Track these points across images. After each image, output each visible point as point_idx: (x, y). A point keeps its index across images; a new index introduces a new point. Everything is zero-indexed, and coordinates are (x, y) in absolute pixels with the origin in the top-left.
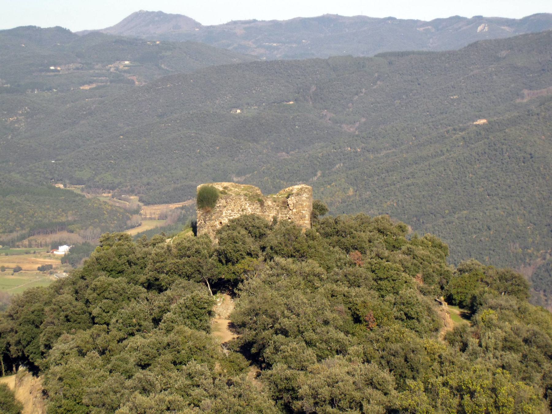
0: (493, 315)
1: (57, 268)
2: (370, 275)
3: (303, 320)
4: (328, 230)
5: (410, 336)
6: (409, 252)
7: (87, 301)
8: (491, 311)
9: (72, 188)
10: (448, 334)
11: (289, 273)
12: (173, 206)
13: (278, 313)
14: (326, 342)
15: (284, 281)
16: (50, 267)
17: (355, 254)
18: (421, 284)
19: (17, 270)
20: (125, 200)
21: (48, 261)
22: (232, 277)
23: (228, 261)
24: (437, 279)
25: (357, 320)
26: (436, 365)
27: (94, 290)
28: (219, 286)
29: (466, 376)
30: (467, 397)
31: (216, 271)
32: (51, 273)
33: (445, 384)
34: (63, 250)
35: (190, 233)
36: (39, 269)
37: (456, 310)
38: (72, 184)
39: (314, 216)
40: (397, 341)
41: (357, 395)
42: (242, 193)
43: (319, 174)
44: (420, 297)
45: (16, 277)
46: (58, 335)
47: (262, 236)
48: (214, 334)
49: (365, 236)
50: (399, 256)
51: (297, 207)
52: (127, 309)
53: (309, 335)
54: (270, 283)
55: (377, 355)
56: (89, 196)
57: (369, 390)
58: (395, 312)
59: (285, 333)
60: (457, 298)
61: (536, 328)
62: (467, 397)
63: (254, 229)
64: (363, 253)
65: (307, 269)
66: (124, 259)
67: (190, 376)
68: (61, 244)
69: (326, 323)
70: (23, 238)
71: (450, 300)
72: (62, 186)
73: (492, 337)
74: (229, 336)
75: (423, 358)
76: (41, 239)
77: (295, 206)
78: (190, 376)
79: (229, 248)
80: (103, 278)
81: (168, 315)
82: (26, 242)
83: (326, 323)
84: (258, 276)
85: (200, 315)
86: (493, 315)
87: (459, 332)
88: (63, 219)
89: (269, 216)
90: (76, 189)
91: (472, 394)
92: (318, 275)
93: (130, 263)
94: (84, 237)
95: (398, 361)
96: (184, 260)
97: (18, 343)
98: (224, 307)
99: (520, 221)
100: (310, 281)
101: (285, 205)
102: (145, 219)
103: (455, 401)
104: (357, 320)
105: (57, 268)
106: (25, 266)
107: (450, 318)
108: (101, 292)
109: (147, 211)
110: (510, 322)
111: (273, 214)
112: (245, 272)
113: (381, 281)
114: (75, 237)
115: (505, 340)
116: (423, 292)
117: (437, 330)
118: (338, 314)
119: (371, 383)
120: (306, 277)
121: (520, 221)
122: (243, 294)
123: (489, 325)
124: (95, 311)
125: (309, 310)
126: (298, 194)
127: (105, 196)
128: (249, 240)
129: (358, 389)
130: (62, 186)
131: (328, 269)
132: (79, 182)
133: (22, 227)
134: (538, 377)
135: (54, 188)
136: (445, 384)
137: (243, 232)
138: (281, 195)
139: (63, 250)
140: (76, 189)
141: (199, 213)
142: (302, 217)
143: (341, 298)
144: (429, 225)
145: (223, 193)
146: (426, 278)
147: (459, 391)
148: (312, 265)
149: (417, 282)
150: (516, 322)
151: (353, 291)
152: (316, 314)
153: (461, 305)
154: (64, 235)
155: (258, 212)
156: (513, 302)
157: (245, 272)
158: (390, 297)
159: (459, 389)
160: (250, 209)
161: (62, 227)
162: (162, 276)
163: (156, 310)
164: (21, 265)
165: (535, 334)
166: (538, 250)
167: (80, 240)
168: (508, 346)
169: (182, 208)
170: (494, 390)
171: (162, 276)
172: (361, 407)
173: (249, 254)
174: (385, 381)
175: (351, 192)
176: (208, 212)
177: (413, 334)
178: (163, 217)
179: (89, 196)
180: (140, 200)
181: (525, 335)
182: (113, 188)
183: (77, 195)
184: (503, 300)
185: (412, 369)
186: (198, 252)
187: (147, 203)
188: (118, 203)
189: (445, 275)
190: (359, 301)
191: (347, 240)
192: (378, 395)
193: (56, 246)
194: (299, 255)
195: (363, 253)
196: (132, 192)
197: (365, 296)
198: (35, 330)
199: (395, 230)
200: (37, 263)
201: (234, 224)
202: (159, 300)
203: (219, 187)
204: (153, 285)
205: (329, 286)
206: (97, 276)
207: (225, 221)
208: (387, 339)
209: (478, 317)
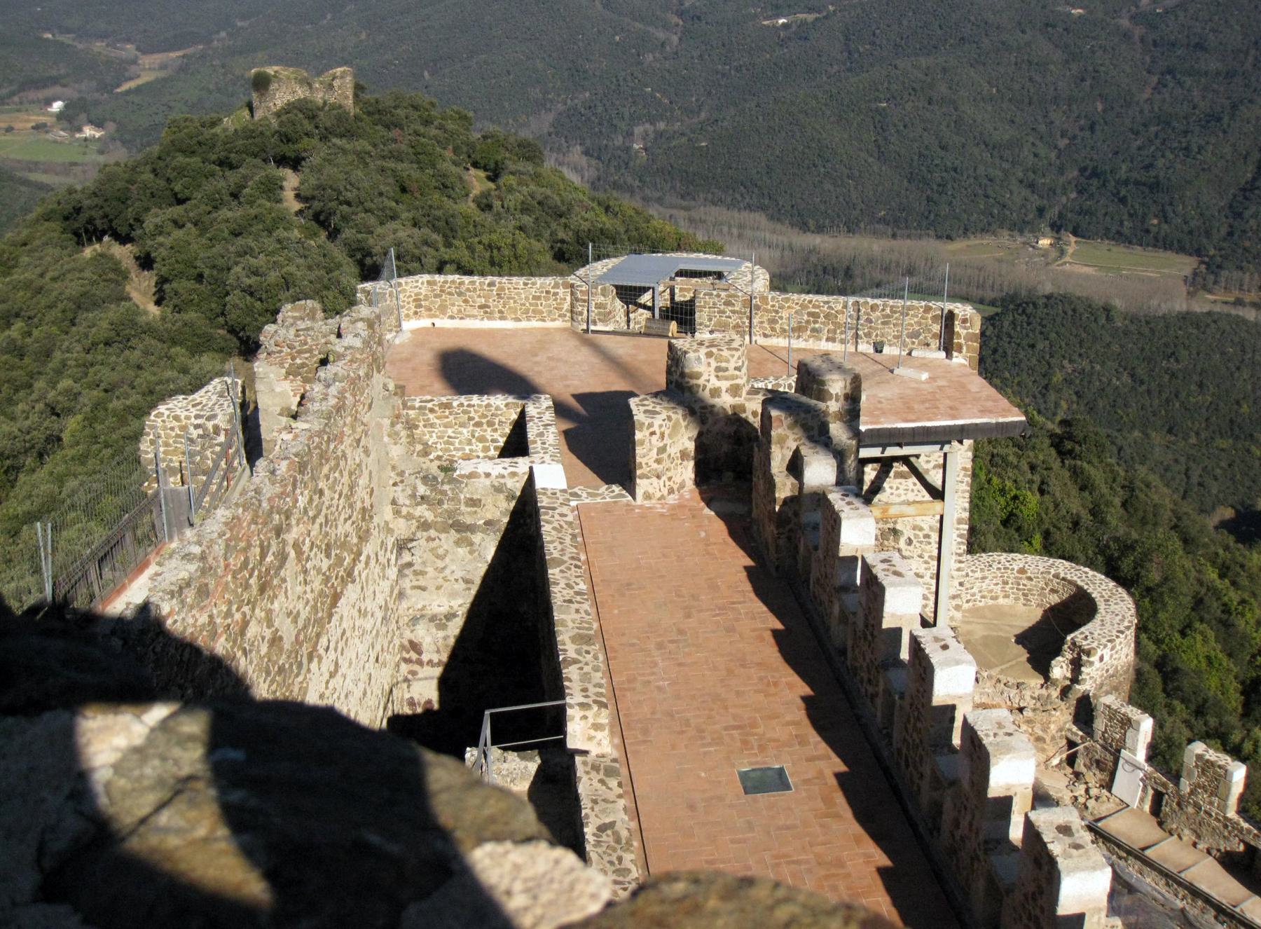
0: (512, 180)
1: (52, 126)
2: (411, 150)
3: (363, 194)
4: (371, 109)
5: (448, 203)
6: (440, 127)
7: (168, 180)
8: (511, 177)
9: (61, 38)
10: (476, 196)
11: (344, 151)
12: (173, 55)
13: (342, 188)
14: (383, 210)
15: (341, 159)
16: (44, 125)
17: (395, 133)
18: (454, 158)
19: (9, 129)
20: (121, 49)
21: (43, 119)
22: (293, 155)
23: (288, 141)
24: (465, 149)
25: (404, 190)
26: (471, 228)
27: (174, 169)
28: (282, 161)
29: (494, 237)
30: (495, 251)
31: (278, 150)
32: (47, 132)
33: (480, 243)
34: (57, 106)
35: (246, 113)
36: (33, 128)
37: (482, 174)
38: (61, 33)
39: (356, 96)
40: (438, 208)
41: (417, 252)
42: (292, 76)
43: (329, 16)
44: (453, 169)
45: (9, 137)
46: (147, 209)
47: (314, 117)
48: (285, 204)
49: (401, 112)
50: (433, 132)
51: (338, 89)
52: (209, 186)
53: (368, 205)
54: (329, 161)
55: (425, 220)
56: (80, 46)
57: (425, 248)
58: (434, 183)
59: (349, 204)
60: (482, 163)
61: (549, 192)
62: (495, 251)
63: (305, 109)
64: (402, 129)
65: (359, 148)
66: (194, 141)
67: (279, 241)
68: (55, 100)
69: (381, 194)
70: (13, 94)
71: (475, 165)
72: (50, 36)
73: (512, 200)
74: (297, 206)
75: (460, 221)
76: (32, 95)
77: (340, 87)
78: (279, 241)
79: (289, 130)
80: (181, 159)
81: (247, 191)
82: (16, 99)
83: (381, 194)
84: (317, 153)
85: (272, 189)
86: (512, 180)
87: (486, 195)
88: (54, 73)
89: (319, 97)
90: (66, 39)
91: (499, 249)
92: (369, 153)
93: (199, 143)
94: (80, 92)
95: (441, 224)
96: (250, 141)
97: (106, 216)
98: (291, 180)
99: (540, 65)
100: (362, 156)
101: (331, 87)
102: (144, 69)
103: (488, 255)
104: (404, 190)
105: (52, 126)
106: (17, 125)
107: (477, 181)
108: (181, 171)
109: (147, 60)
110: (527, 186)
111: (320, 95)
112: (305, 150)
113: (421, 157)
114: (67, 91)
115: (523, 202)
116: (455, 164)
117: (467, 195)
118: (389, 187)
119: (426, 243)
120: (358, 154)
121: (540, 65)
122: (307, 170)
123: (510, 190)
124: (178, 188)
125: (366, 185)
126: (342, 77)
127: (98, 46)
128: (306, 122)
129: (417, 247)
130: (50, 36)
131: (375, 146)
132: (68, 31)
133: (11, 82)
134: (547, 234)
135: (41, 39)
136: (480, 243)
137: (301, 116)
138: (326, 77)
139: (57, 106)
140: (66, 39)
141: (254, 95)
142: (347, 97)
143: (389, 172)
144: (447, 71)
145: (275, 76)
146: (456, 150)
147: (490, 247)
148: (362, 144)
149: (449, 154)
150: (533, 187)
151: (400, 166)
152: (372, 188)
153: (485, 169)
154: (58, 89)
155: (307, 94)
156: (530, 168)
157: (305, 150)
158: (430, 171)
159: (490, 246)
160: (301, 93)
161: (55, 81)
162: (233, 155)
163: (233, 186)
164: (12, 125)
165: (547, 197)
166: (559, 95)
167: (76, 95)
168: (525, 209)
169: (184, 56)
170: (513, 246)
171: (233, 155)
172: (420, 260)
173: (306, 134)
174: (436, 241)
175: (363, 36)
176: (262, 95)
177: (451, 202)
178: (163, 67)
179: (80, 46)
180: (138, 49)
181: (539, 197)
182: (106, 37)
183: (68, 46)
184: (522, 166)
185: (452, 230)
186: (262, 133)
187: (144, 53)
188: (114, 53)
189: (471, 146)
190: (405, 174)
191: (387, 118)
192: (431, 251)
193: (49, 102)
194: (349, 134)
195: (402, 129)
196: (128, 40)
197: (407, 169)
198: (123, 206)
199: (428, 107)
200: (28, 121)
201: (289, 108)
202: (233, 177)
203: (270, 70)
204: (225, 164)
205: (379, 163)
206: (174, 158)
207: (279, 103)
208: (431, 207)
209: (501, 181)
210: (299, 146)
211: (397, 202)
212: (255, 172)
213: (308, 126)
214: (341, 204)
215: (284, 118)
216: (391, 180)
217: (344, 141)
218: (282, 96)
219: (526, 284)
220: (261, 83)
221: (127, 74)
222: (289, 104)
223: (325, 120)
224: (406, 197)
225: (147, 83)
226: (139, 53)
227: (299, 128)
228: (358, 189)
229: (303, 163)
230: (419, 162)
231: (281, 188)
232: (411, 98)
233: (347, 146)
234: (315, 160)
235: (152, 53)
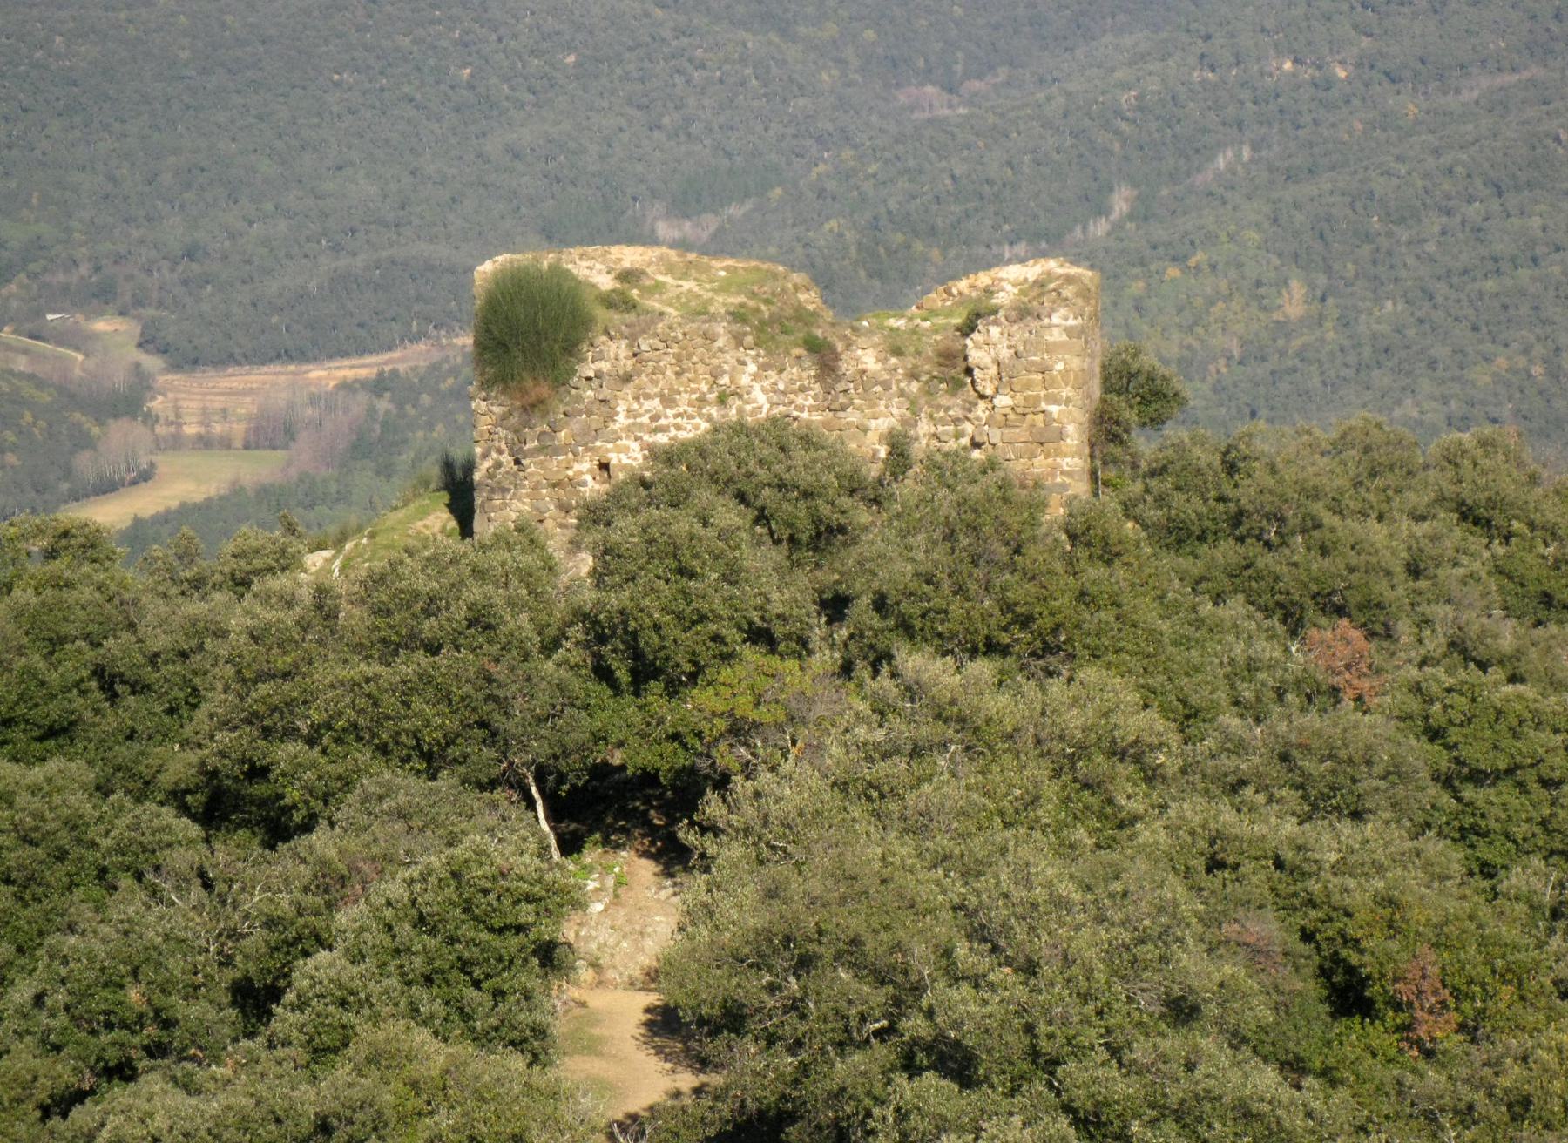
2: (1420, 754)
3: (1055, 996)
4: (1188, 507)
11: (977, 737)
12: (325, 375)
13: (921, 958)
15: (949, 784)
20: (63, 338)
22: (665, 760)
23: (644, 671)
25: (1349, 996)
28: (593, 805)
35: (439, 520)
39: (1107, 432)
42: (722, 303)
43: (1120, 203)
51: (1008, 378)
54: (874, 793)
63: (791, 500)
65: (1074, 721)
66: (76, 662)
69: (1182, 1011)
79: (649, 601)
81: (322, 966)
83: (1182, 1011)
84: (806, 746)
85: (493, 963)
89: (867, 431)
92: (1133, 753)
93: (108, 681)
96: (410, 665)
98: (626, 921)
100: (1090, 778)
101: (954, 369)
102: (176, 443)
104: (1349, 996)
109: (188, 399)
111: (885, 419)
118: (1243, 966)
120: (1068, 760)
125: (1088, 942)
126: (1022, 313)
128: (760, 559)
131: (1189, 717)
137: (730, 515)
138: (928, 317)
141: (487, 410)
142: (1047, 438)
143: (1258, 879)
145: (611, 301)
148: (1098, 697)
151: (1329, 841)
155: (807, 410)
157: (739, 731)
160: (763, 391)
162: (285, 753)
169: (379, 386)
171: (285, 753)
173: (760, 636)
175: (1294, 302)
176: (534, 408)
178: (271, 432)
186: (480, 621)
190: (1360, 893)
194: (1032, 640)
196: (102, 296)
201: (675, 475)
202: (269, 882)
203: (593, 269)
204: (238, 804)
205: (1191, 809)
207: (629, 457)
210: (702, 704)
211: (1294, 1068)
212: (409, 843)
213: (785, 592)
214: (910, 1067)
215: (625, 529)
216: (1268, 928)
217: (983, 668)
218: (635, 417)
219: (1402, 893)
220: (530, 341)
221: (84, 463)
222: (667, 457)
223: (885, 554)
224: (1355, 1039)
225: (185, 512)
226: (151, 362)
227: (708, 587)
228: (1030, 969)
229: (712, 806)
230: (1467, 834)
231: (549, 956)
232: (1451, 459)
233: (997, 704)
234: (789, 786)
235: (225, 360)
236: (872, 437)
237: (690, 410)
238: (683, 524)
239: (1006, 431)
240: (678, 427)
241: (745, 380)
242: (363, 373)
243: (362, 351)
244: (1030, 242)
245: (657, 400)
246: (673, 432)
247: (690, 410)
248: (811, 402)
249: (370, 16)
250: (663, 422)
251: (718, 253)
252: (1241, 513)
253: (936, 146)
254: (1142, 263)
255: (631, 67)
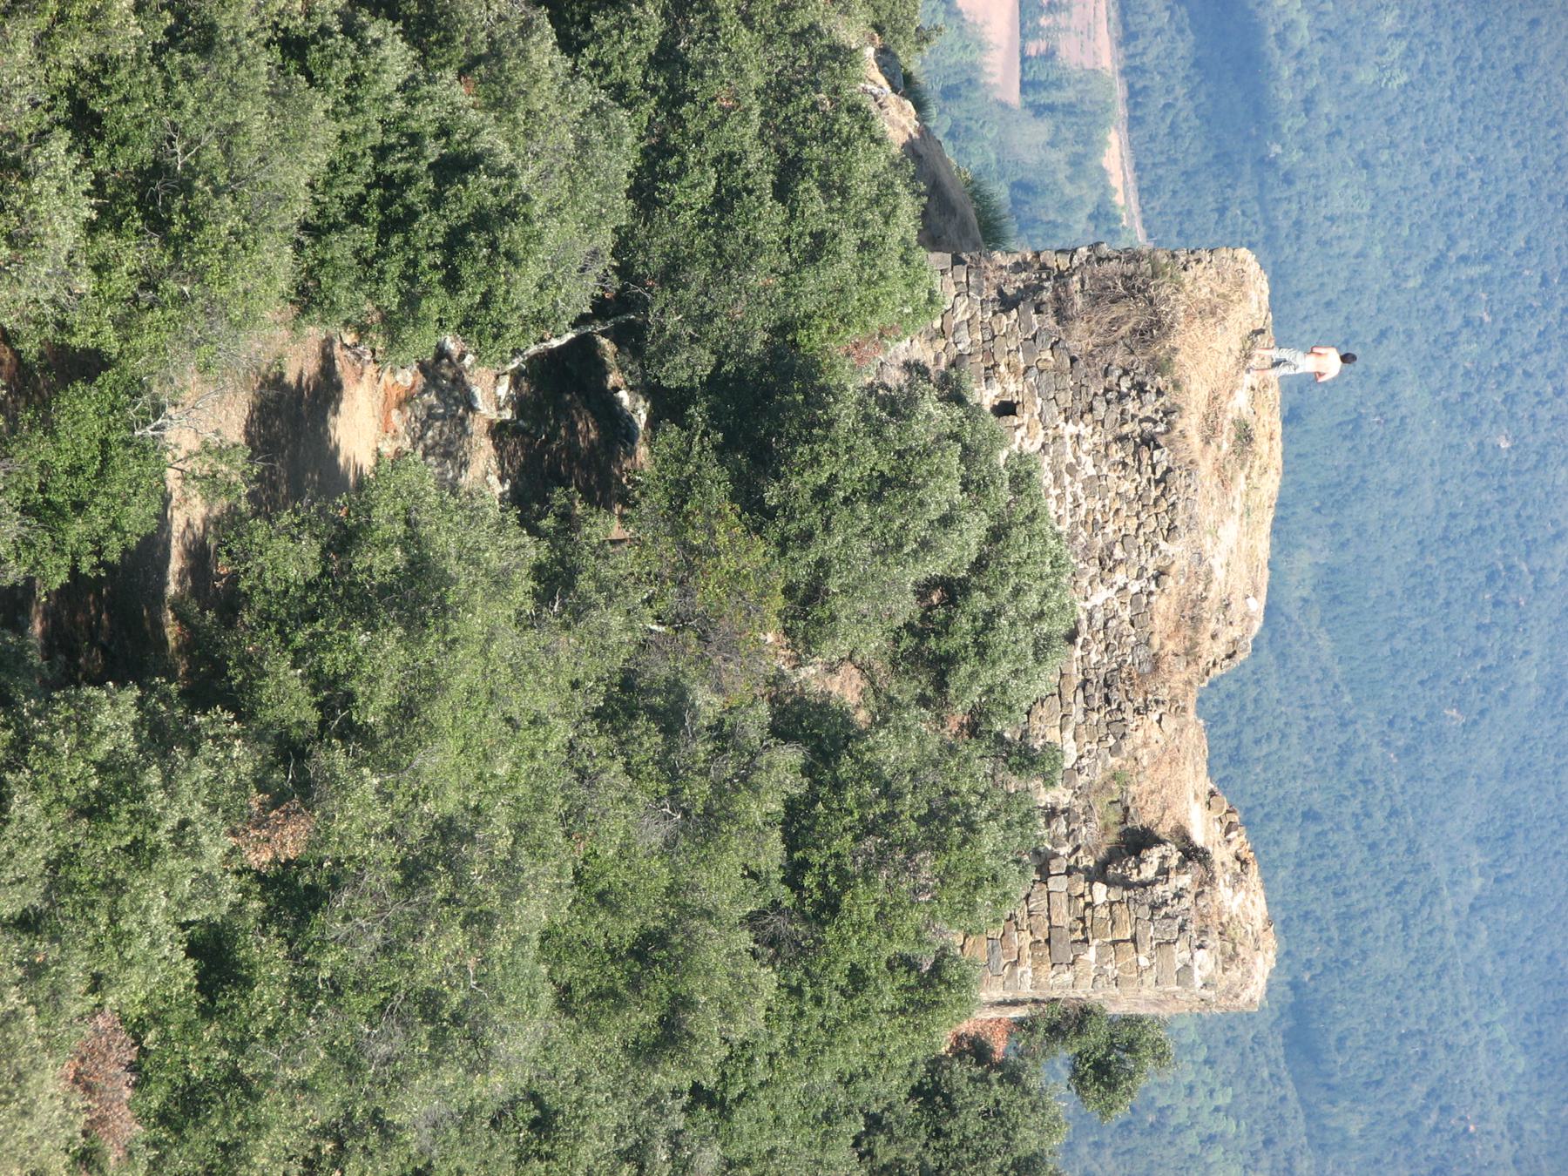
236: (1053, 735)
237: (1082, 512)
238: (945, 492)
239: (1064, 897)
240: (1060, 498)
241: (1120, 577)
242: (1119, 199)
243: (1147, 192)
244: (1292, 1006)
245: (1092, 472)
246: (1054, 492)
247: (1082, 512)
248: (1094, 658)
249: (1550, 198)
250: (1067, 479)
251: (1269, 610)
252: (517, 264)
253: (1407, 889)
254: (1268, 1142)
255: (1495, 516)
